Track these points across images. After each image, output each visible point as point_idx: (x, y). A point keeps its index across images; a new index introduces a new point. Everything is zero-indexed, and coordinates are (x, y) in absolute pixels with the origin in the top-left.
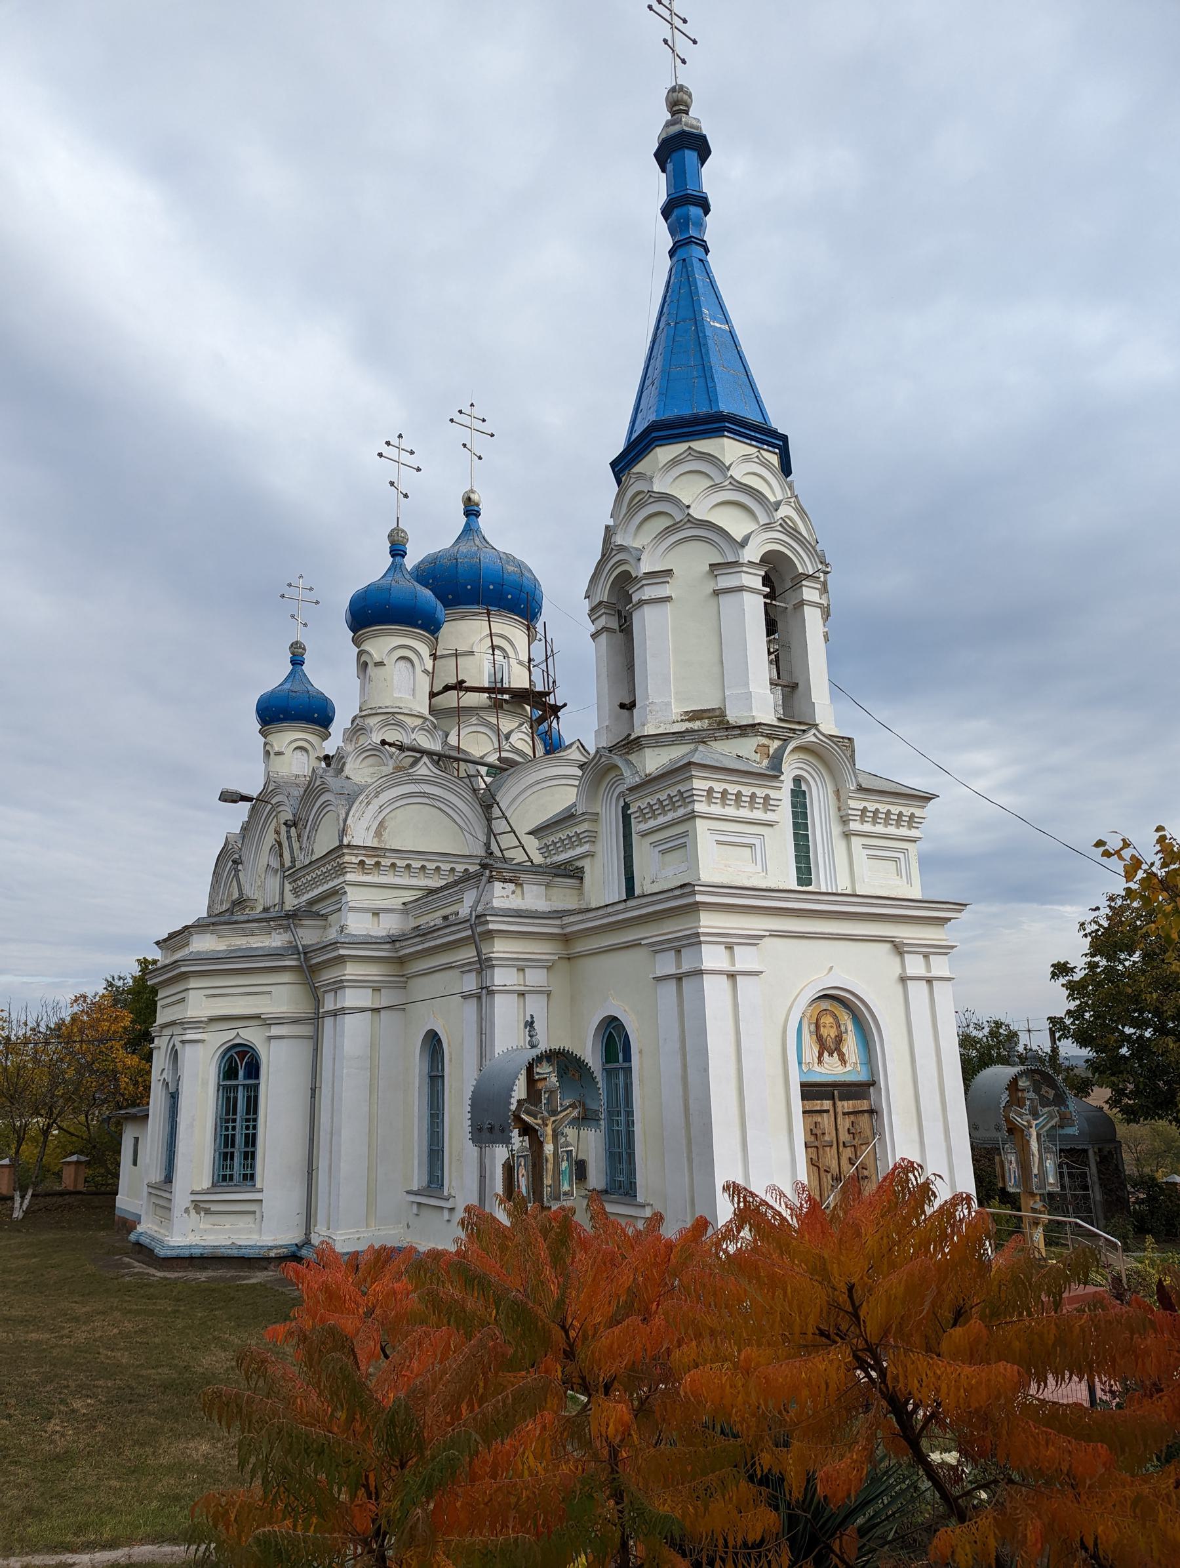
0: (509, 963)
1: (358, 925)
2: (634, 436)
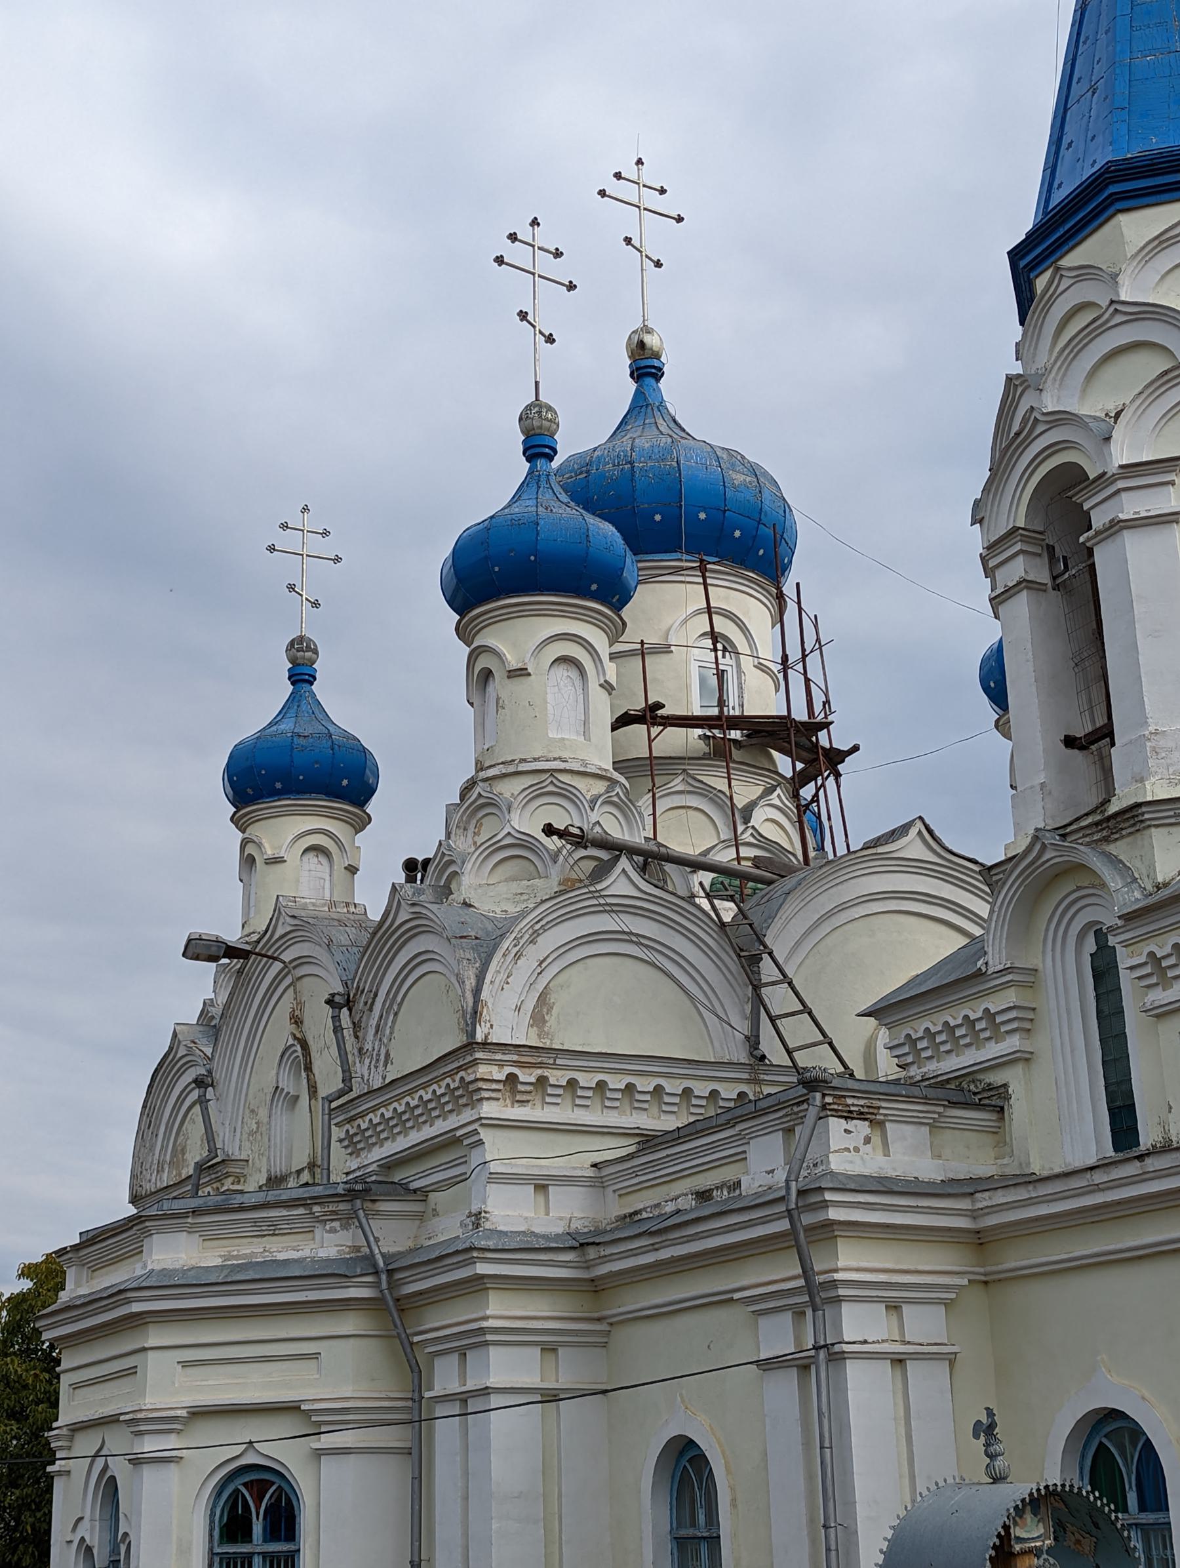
1: (510, 1211)
2: (1058, 197)
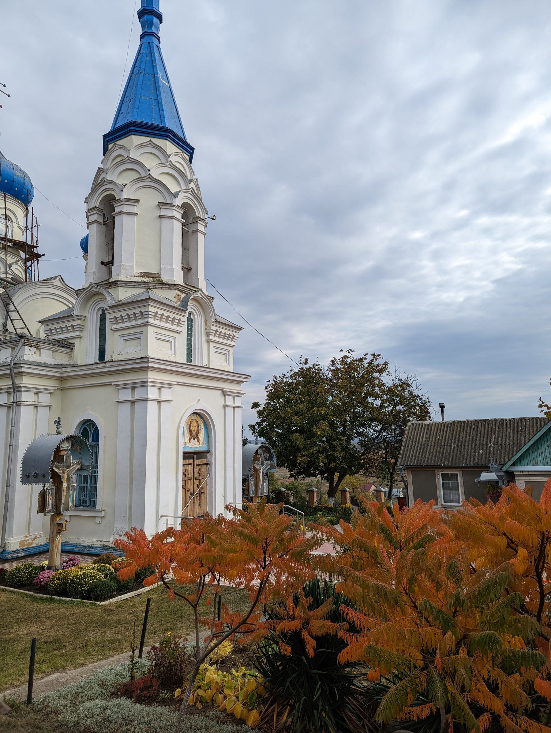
0: (30, 389)
